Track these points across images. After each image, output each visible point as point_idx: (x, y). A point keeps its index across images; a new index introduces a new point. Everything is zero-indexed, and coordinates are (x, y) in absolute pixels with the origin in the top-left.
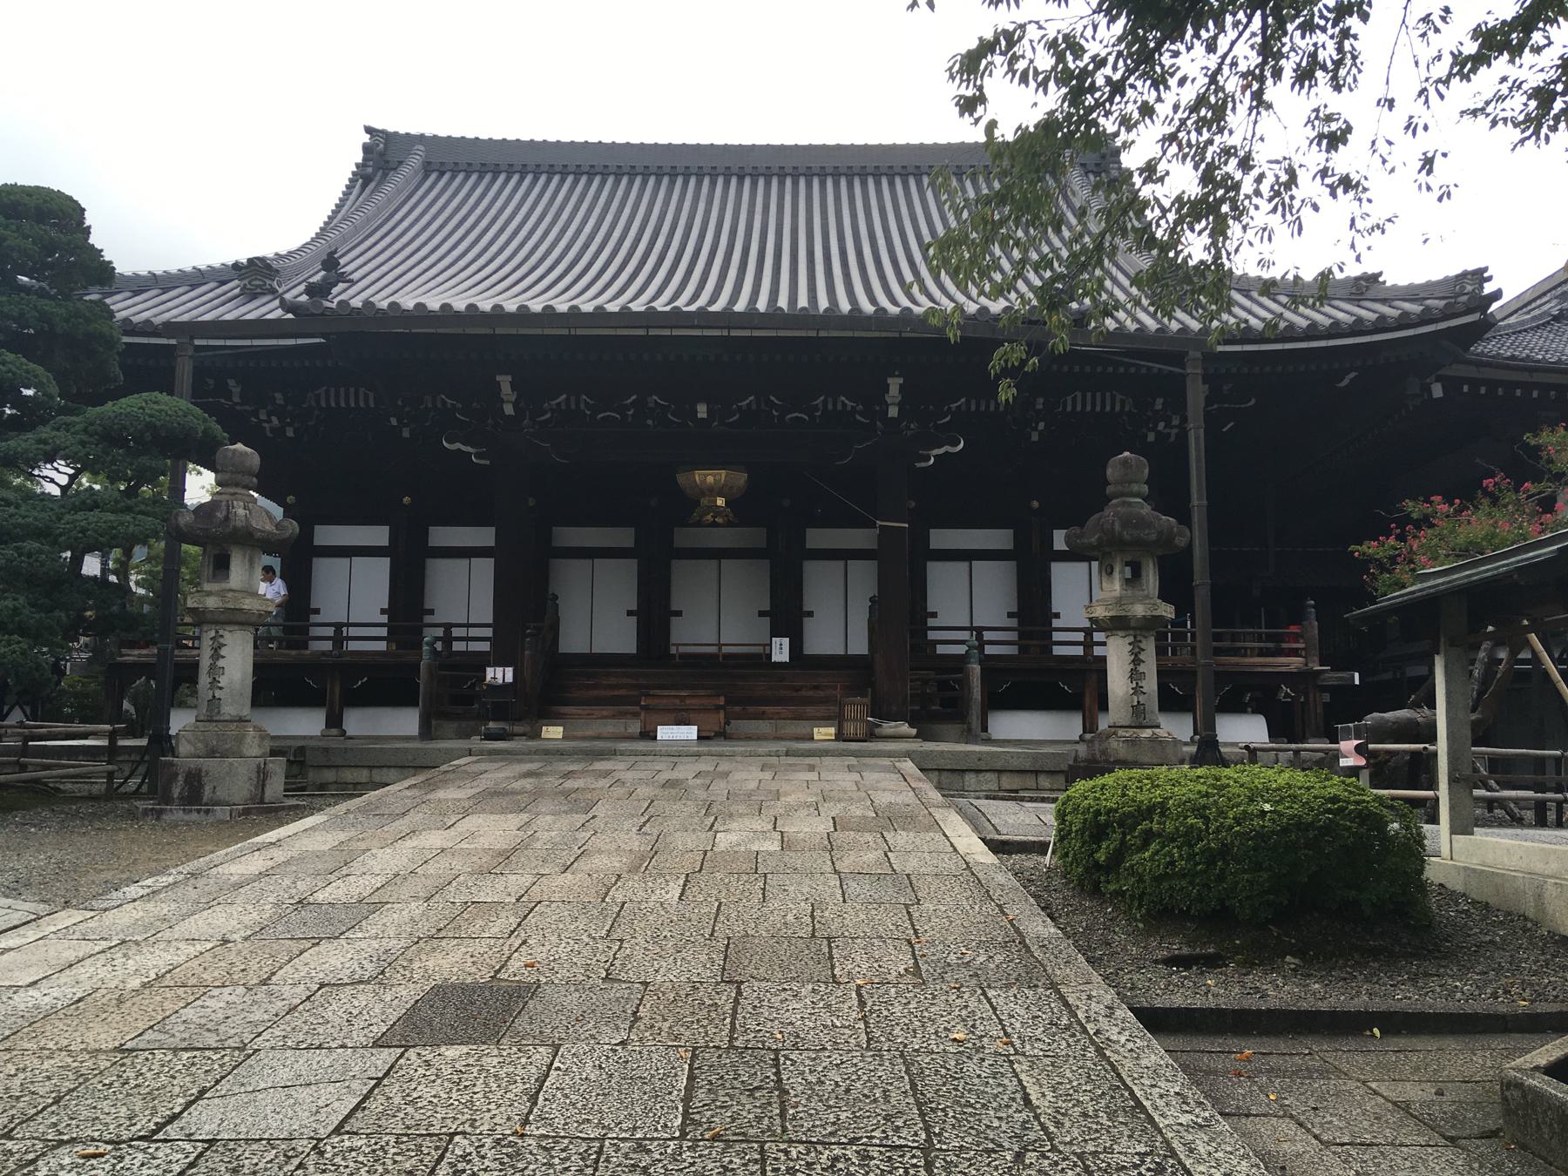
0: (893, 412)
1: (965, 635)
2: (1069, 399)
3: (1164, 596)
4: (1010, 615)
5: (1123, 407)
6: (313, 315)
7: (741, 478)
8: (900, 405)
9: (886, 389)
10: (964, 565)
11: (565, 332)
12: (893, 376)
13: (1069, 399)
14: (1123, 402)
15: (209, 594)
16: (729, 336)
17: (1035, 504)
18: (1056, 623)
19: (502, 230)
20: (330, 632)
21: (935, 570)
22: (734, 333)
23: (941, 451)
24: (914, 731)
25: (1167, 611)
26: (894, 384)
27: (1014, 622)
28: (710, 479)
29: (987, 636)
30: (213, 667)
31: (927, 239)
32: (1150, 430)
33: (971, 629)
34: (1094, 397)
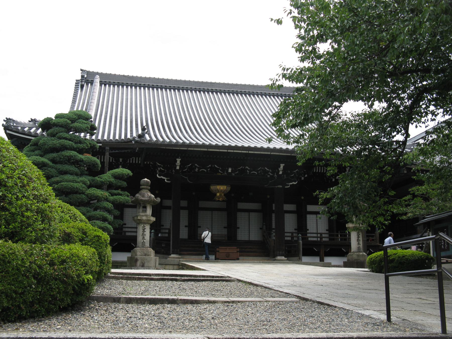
0: (178, 168)
1: (315, 235)
2: (131, 159)
3: (153, 215)
4: (295, 229)
5: (112, 160)
6: (142, 143)
7: (229, 189)
8: (180, 166)
9: (280, 167)
10: (247, 214)
11: (206, 150)
12: (178, 158)
13: (131, 159)
14: (112, 159)
15: (143, 216)
16: (227, 152)
17: (303, 198)
18: (308, 232)
19: (217, 124)
20: (290, 234)
21: (308, 216)
22: (250, 152)
23: (291, 184)
24: (286, 259)
25: (153, 219)
26: (282, 166)
27: (328, 232)
28: (222, 188)
29: (323, 235)
30: (143, 234)
31: (270, 123)
32: (303, 176)
33: (317, 233)
34: (138, 159)
